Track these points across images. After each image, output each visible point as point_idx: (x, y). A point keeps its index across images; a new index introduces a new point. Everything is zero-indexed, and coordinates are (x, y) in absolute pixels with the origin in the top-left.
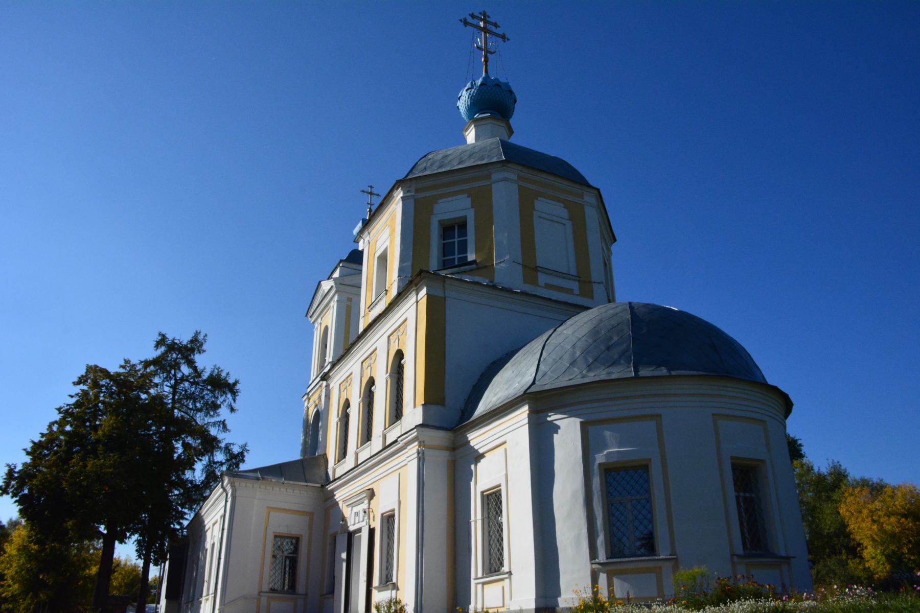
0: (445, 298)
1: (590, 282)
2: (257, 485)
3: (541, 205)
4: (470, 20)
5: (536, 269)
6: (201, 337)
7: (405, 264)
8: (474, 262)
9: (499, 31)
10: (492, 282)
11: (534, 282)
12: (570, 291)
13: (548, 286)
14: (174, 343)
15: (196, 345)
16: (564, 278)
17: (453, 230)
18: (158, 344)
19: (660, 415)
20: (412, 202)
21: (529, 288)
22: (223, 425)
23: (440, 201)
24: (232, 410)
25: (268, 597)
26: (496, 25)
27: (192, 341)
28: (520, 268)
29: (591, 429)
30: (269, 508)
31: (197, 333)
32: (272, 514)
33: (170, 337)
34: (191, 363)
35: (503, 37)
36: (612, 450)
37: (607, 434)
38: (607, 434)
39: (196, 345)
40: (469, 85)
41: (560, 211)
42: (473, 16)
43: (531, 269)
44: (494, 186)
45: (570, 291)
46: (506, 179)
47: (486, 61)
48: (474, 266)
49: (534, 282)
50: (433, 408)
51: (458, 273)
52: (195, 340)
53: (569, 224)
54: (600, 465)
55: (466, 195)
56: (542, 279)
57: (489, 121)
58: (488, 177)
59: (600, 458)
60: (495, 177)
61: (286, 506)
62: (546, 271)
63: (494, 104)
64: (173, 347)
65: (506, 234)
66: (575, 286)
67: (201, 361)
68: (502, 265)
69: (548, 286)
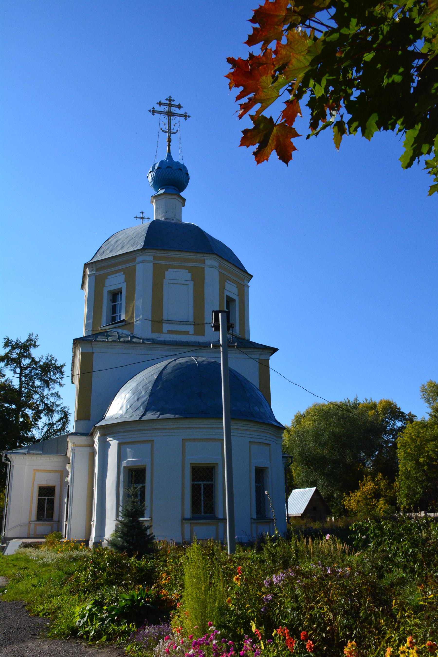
0: (93, 353)
1: (203, 324)
2: (27, 457)
3: (170, 274)
4: (158, 108)
5: (162, 321)
6: (33, 338)
7: (89, 322)
8: (124, 321)
9: (181, 111)
10: (132, 334)
11: (160, 331)
12: (187, 333)
13: (170, 332)
14: (17, 344)
15: (31, 343)
16: (187, 324)
17: (115, 295)
18: (6, 345)
19: (153, 441)
20: (93, 277)
21: (155, 336)
22: (57, 395)
23: (109, 277)
24: (61, 385)
25: (35, 524)
26: (179, 107)
27: (27, 341)
28: (150, 323)
29: (122, 447)
30: (34, 470)
31: (30, 335)
32: (38, 474)
33: (13, 339)
34: (29, 356)
35: (185, 116)
36: (130, 460)
37: (128, 450)
38: (128, 450)
39: (31, 343)
40: (151, 170)
41: (185, 275)
42: (160, 104)
43: (157, 322)
44: (137, 266)
45: (187, 333)
46: (144, 261)
47: (170, 141)
48: (123, 323)
49: (160, 331)
50: (82, 422)
51: (115, 328)
52: (29, 340)
53: (191, 284)
54: (124, 467)
55: (122, 273)
56: (166, 327)
57: (163, 197)
58: (135, 259)
59: (124, 464)
60: (139, 259)
61: (48, 469)
62: (169, 322)
63: (171, 179)
64: (16, 346)
65: (141, 301)
66: (191, 329)
67: (35, 353)
68: (138, 322)
69: (170, 332)
